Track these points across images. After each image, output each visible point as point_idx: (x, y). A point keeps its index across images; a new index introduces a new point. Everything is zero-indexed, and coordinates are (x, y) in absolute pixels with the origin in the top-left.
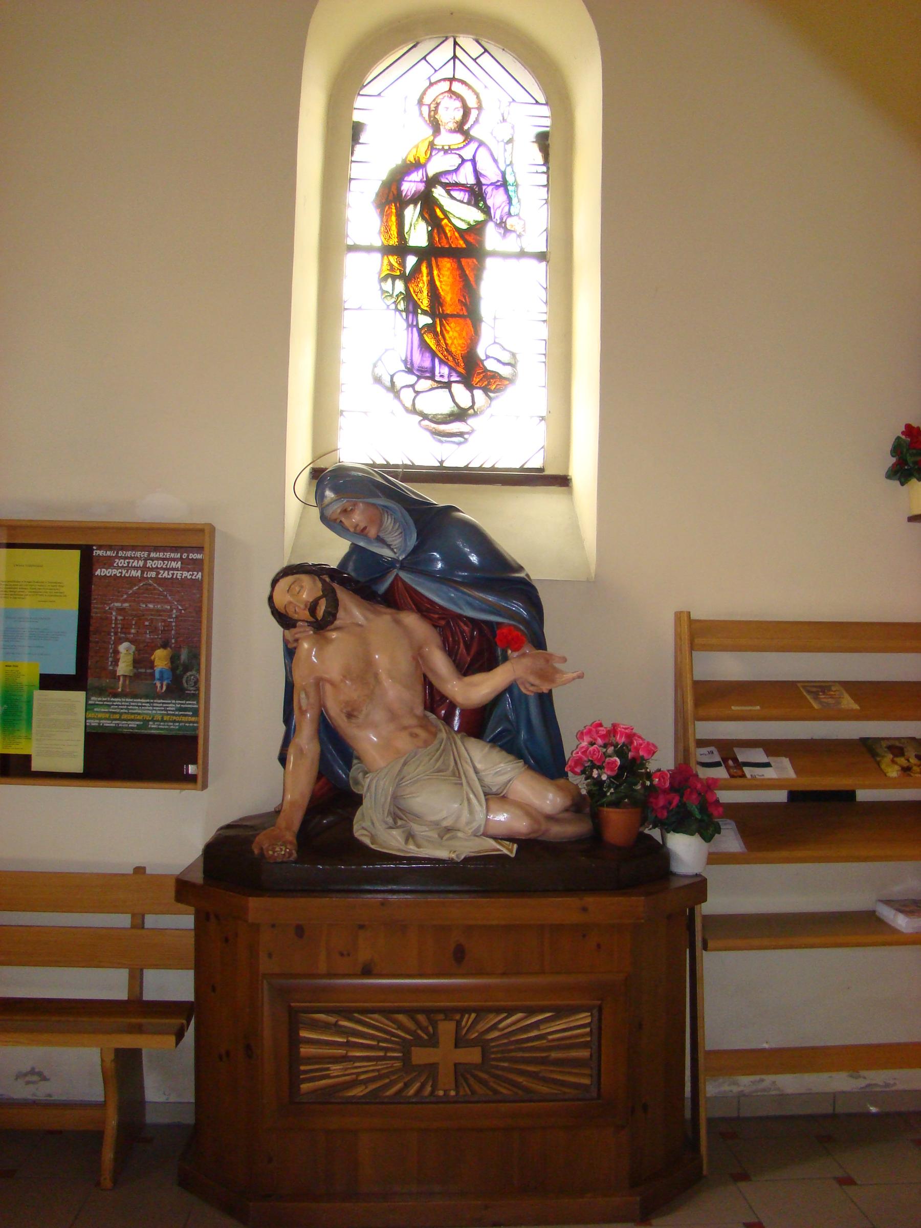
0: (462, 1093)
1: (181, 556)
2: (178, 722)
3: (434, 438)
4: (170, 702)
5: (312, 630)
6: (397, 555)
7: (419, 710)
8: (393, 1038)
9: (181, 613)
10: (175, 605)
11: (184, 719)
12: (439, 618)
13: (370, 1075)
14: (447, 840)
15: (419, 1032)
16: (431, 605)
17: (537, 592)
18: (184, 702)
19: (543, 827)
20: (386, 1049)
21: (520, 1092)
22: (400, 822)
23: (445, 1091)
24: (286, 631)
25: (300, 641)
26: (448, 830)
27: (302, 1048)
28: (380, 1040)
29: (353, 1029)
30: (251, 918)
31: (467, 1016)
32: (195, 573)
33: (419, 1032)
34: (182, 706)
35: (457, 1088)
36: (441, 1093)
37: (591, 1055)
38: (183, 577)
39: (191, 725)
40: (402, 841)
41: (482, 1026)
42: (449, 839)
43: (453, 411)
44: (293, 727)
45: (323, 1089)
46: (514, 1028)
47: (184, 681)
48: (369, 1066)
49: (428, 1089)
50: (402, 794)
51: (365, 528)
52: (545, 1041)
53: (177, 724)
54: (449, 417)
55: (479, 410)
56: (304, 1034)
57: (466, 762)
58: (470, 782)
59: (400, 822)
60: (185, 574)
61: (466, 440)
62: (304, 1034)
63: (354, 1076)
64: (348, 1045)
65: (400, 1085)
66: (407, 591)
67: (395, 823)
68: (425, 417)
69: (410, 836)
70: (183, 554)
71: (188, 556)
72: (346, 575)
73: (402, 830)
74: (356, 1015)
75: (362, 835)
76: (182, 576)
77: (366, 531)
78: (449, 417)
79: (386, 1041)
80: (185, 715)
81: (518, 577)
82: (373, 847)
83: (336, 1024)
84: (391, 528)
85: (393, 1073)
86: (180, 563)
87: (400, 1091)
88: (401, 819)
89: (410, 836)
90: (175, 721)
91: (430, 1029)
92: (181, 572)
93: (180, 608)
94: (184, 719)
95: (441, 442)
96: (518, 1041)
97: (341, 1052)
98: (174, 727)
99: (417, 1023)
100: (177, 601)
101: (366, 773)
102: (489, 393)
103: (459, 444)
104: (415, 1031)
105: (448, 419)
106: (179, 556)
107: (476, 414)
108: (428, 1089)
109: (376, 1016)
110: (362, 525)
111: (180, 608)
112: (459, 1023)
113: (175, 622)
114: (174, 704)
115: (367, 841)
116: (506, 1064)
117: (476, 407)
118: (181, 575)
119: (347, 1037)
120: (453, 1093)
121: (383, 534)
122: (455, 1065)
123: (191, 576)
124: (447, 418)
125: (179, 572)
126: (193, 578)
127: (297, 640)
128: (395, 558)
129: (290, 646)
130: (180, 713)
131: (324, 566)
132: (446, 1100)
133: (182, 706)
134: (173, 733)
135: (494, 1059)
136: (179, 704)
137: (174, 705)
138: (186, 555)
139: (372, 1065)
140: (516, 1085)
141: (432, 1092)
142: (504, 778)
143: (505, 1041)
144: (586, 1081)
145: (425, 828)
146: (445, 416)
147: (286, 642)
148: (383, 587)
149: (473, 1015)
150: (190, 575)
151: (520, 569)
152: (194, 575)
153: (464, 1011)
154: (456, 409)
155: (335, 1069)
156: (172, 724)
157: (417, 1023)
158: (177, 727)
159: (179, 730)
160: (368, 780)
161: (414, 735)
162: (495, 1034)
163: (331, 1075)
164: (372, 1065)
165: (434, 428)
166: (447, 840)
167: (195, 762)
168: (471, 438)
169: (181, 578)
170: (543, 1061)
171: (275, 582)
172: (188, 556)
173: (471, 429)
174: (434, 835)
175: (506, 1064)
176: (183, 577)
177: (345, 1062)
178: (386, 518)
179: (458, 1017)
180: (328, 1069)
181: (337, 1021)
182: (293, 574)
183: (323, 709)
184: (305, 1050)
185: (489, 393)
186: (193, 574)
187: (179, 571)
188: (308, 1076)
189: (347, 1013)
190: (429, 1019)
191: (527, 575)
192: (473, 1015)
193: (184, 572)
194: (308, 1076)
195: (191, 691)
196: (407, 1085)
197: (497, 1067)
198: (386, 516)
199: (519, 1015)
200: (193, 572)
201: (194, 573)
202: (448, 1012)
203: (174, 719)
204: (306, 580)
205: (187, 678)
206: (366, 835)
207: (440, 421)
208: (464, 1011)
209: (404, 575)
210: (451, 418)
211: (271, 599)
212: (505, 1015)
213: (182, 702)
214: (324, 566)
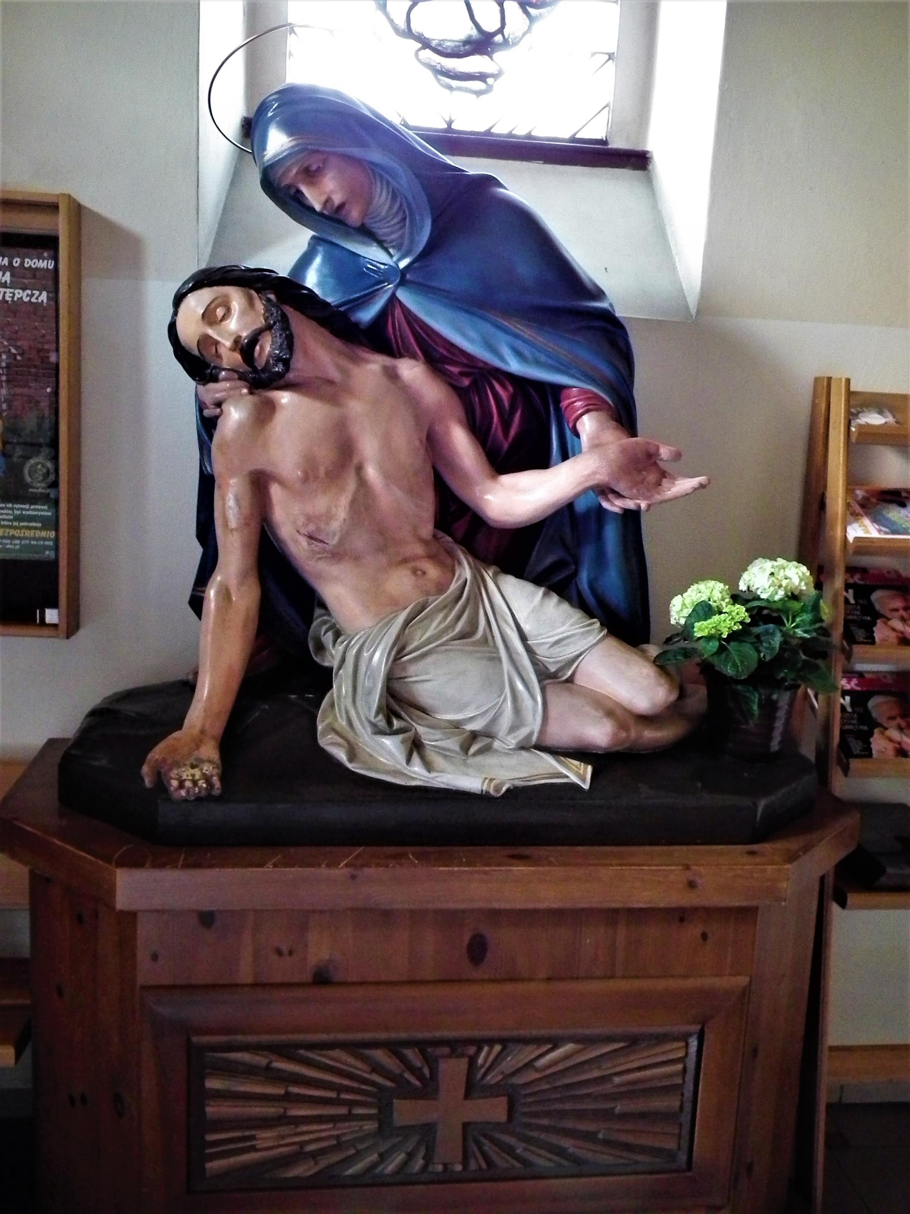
0: (473, 1166)
1: (10, 263)
2: (19, 538)
3: (438, 80)
4: (4, 505)
5: (247, 388)
6: (395, 259)
7: (427, 530)
8: (363, 1087)
9: (15, 359)
10: (5, 346)
11: (28, 533)
12: (462, 374)
13: (325, 1144)
14: (474, 755)
15: (407, 1075)
16: (448, 351)
17: (628, 337)
18: (27, 507)
19: (633, 734)
20: (351, 1104)
21: (565, 1163)
22: (396, 724)
23: (445, 1165)
24: (200, 387)
25: (224, 406)
26: (474, 736)
27: (208, 1105)
28: (340, 1089)
29: (298, 1075)
30: (122, 902)
31: (486, 1049)
32: (37, 293)
33: (407, 1075)
34: (24, 513)
35: (465, 1162)
36: (440, 1168)
37: (681, 1107)
38: (15, 299)
39: (42, 543)
40: (401, 757)
41: (511, 1062)
42: (480, 752)
43: (470, 36)
44: (395, 345)
45: (245, 1167)
46: (560, 1067)
47: (26, 472)
48: (321, 1131)
49: (419, 1163)
50: (403, 675)
51: (341, 206)
52: (610, 1086)
53: (18, 542)
54: (464, 46)
55: (511, 36)
56: (213, 1084)
57: (506, 621)
58: (514, 656)
59: (396, 724)
60: (19, 293)
61: (489, 89)
62: (213, 1084)
63: (295, 1148)
64: (288, 1097)
65: (374, 1157)
66: (409, 323)
67: (390, 723)
68: (426, 44)
69: (416, 746)
70: (13, 258)
71: (22, 263)
72: (304, 292)
73: (401, 737)
74: (302, 1052)
75: (333, 744)
76: (13, 297)
77: (344, 212)
78: (464, 46)
79: (348, 1089)
80: (30, 528)
81: (596, 309)
82: (350, 766)
83: (268, 1068)
84: (386, 207)
85: (362, 1139)
86: (8, 274)
87: (374, 1166)
88: (399, 717)
89: (416, 746)
90: (13, 537)
91: (426, 1071)
92: (12, 290)
93: (13, 351)
94: (28, 533)
95: (450, 88)
96: (568, 1086)
97: (271, 1110)
98: (13, 547)
99: (403, 1059)
100: (8, 340)
101: (338, 634)
102: (527, 7)
103: (479, 93)
104: (401, 1076)
105: (462, 48)
106: (6, 261)
107: (506, 43)
108: (419, 1163)
109: (336, 1053)
110: (337, 199)
111: (13, 351)
112: (472, 1060)
113: (7, 375)
114: (9, 509)
115: (341, 755)
116: (545, 1122)
117: (506, 32)
118: (11, 295)
119: (287, 1087)
120: (459, 1168)
121: (371, 221)
122: (466, 1126)
123: (28, 298)
124: (459, 46)
125: (8, 290)
126: (33, 300)
127: (219, 404)
128: (392, 264)
129: (206, 413)
130: (22, 524)
131: (267, 273)
132: (447, 1178)
133: (24, 513)
134: (12, 556)
135: (525, 1114)
136: (18, 509)
137: (10, 512)
138: (19, 260)
139: (329, 1130)
140: (560, 1152)
141: (425, 1168)
142: (569, 652)
143: (546, 1087)
144: (670, 1144)
145: (438, 735)
146: (456, 43)
147: (201, 407)
148: (367, 315)
149: (498, 1048)
150: (28, 295)
151: (598, 294)
152: (35, 296)
153: (479, 1043)
154: (474, 33)
155: (266, 1137)
156: (9, 541)
157: (403, 1059)
158: (18, 547)
159: (20, 551)
160: (341, 648)
161: (419, 573)
162: (533, 1076)
163: (257, 1147)
164: (329, 1130)
165: (439, 63)
166: (474, 755)
167: (55, 605)
168: (498, 85)
169: (13, 301)
170: (607, 1115)
171: (179, 299)
172: (22, 263)
173: (498, 68)
174: (452, 744)
175: (545, 1122)
176: (15, 299)
177: (280, 1125)
178: (379, 190)
179: (472, 1050)
180: (253, 1138)
181: (270, 1062)
182: (211, 284)
183: (264, 525)
184: (213, 1110)
185: (527, 7)
186: (33, 295)
187: (7, 287)
188: (219, 1149)
189: (285, 1051)
190: (423, 1053)
191: (611, 305)
192: (498, 1048)
193: (16, 291)
194: (219, 1149)
195: (37, 488)
196: (383, 1157)
197: (529, 1126)
198: (379, 184)
199: (568, 1047)
200: (32, 290)
201: (34, 292)
202: (455, 1046)
203: (11, 534)
204: (236, 297)
205: (31, 467)
206: (339, 745)
207: (449, 51)
208: (479, 1043)
209: (403, 296)
210: (467, 47)
211: (172, 329)
212: (549, 1046)
213: (23, 506)
214: (267, 273)
